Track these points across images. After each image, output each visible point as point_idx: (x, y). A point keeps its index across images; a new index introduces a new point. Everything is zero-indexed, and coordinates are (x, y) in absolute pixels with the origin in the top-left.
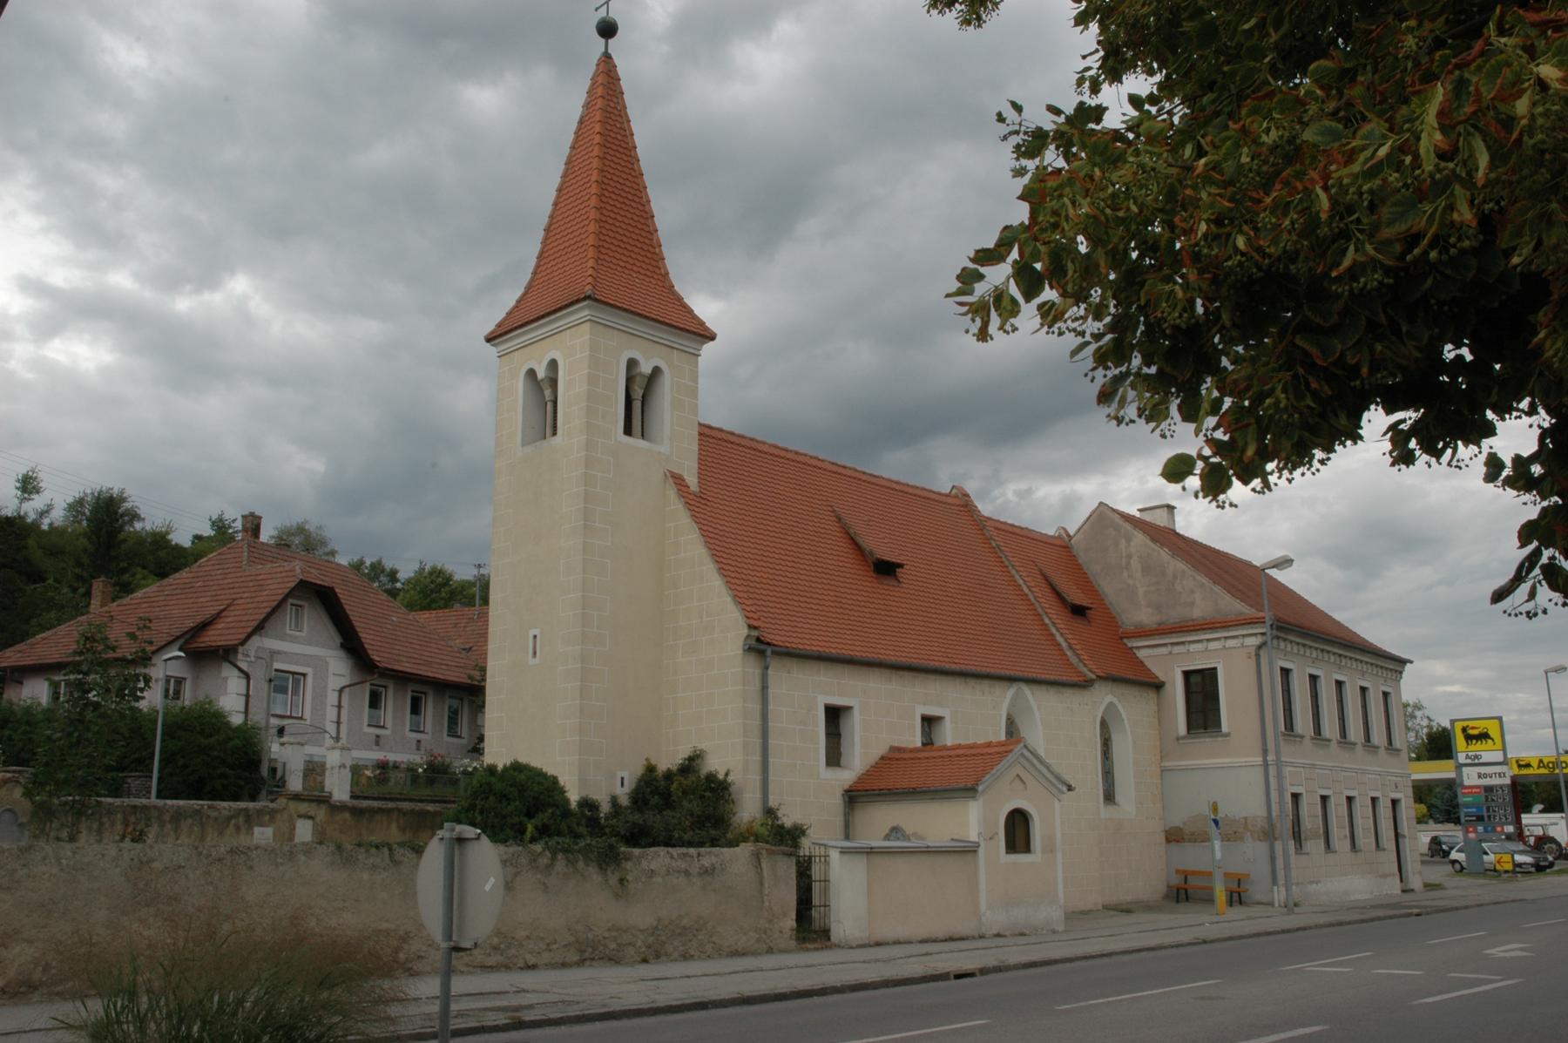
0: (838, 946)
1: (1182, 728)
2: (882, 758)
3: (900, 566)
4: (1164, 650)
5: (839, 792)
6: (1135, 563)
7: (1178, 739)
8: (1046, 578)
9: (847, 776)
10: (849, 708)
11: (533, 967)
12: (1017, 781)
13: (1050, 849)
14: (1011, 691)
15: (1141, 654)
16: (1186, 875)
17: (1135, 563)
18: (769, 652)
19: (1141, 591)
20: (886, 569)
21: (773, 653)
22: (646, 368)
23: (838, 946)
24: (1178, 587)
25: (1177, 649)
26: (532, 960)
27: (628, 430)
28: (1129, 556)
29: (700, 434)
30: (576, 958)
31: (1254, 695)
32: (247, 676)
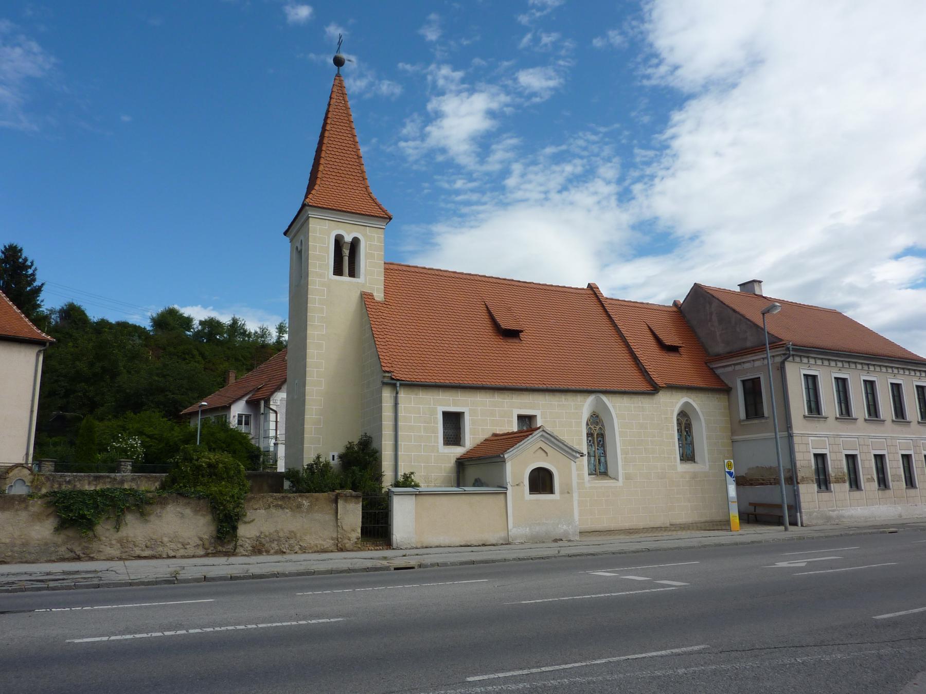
0: (398, 548)
1: (742, 415)
2: (486, 440)
3: (522, 331)
4: (730, 369)
5: (453, 461)
6: (714, 318)
7: (740, 421)
8: (650, 329)
9: (458, 451)
10: (535, 416)
11: (174, 557)
12: (540, 451)
13: (568, 491)
14: (591, 399)
15: (719, 372)
16: (755, 505)
17: (714, 318)
18: (398, 384)
19: (718, 334)
20: (512, 334)
21: (401, 385)
22: (348, 238)
23: (398, 548)
24: (738, 330)
25: (738, 367)
26: (172, 554)
27: (338, 271)
28: (711, 314)
29: (385, 269)
30: (202, 553)
31: (32, 378)
32: (276, 412)
